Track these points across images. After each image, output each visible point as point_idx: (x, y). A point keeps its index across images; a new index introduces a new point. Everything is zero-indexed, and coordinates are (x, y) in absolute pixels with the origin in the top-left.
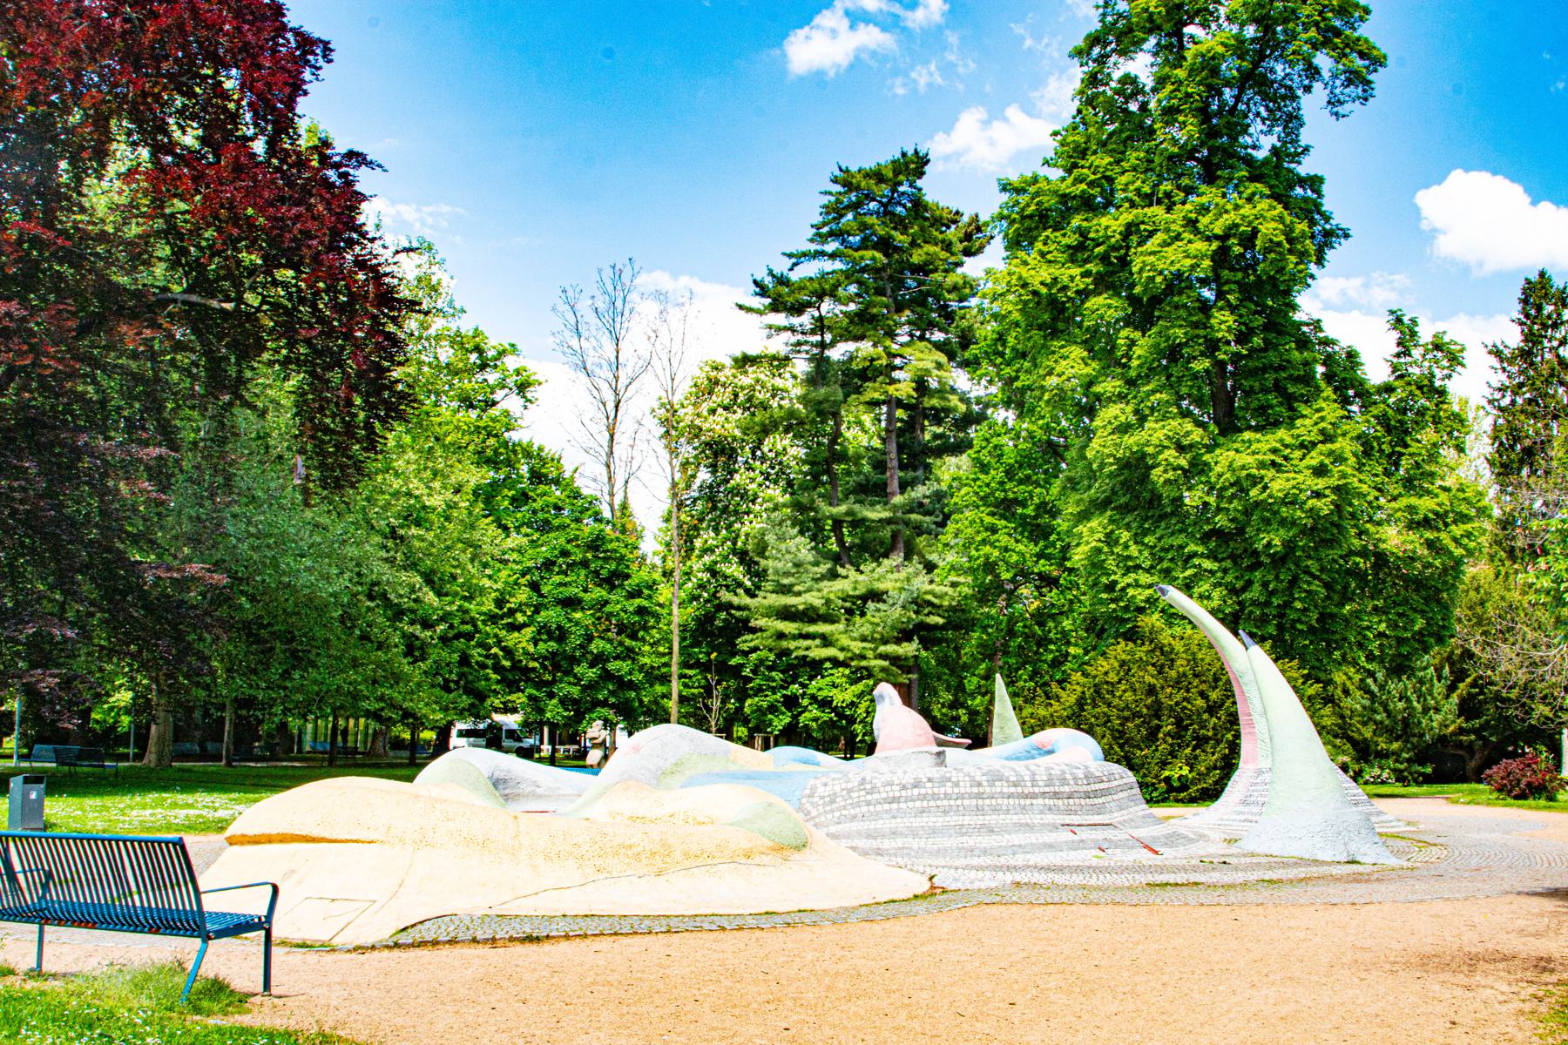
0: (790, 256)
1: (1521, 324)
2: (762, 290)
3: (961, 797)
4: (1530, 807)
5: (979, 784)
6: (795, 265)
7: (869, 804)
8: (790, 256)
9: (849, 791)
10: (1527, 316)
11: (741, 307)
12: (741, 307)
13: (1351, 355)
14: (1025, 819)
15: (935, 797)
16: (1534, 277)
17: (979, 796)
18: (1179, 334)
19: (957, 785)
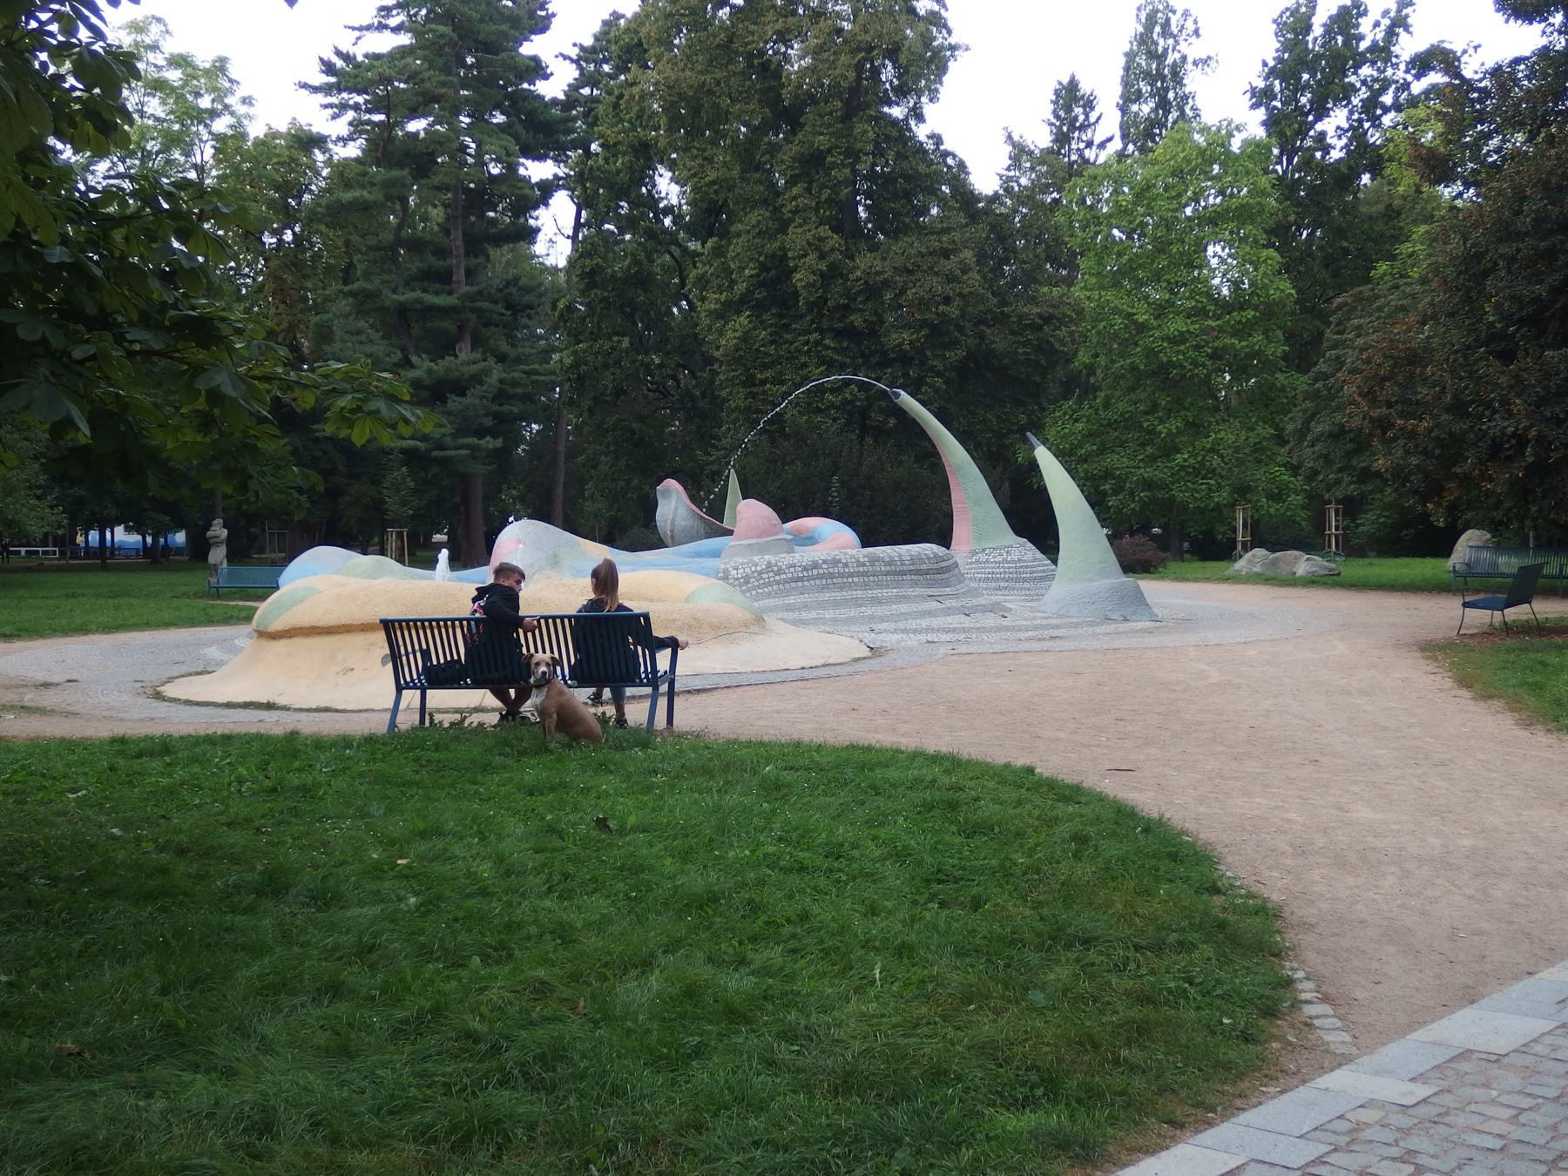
0: (354, 29)
1: (1051, 124)
2: (328, 68)
3: (851, 575)
4: (655, 566)
5: (864, 565)
6: (359, 38)
7: (778, 583)
8: (354, 29)
9: (760, 573)
10: (1057, 117)
11: (305, 86)
12: (305, 86)
13: (962, 165)
14: (902, 592)
15: (831, 576)
16: (1065, 81)
17: (864, 574)
18: (822, 141)
19: (846, 565)
